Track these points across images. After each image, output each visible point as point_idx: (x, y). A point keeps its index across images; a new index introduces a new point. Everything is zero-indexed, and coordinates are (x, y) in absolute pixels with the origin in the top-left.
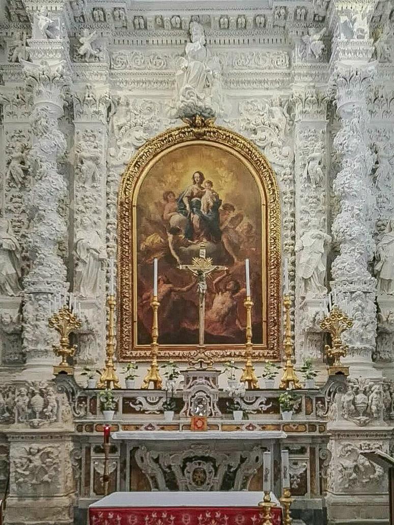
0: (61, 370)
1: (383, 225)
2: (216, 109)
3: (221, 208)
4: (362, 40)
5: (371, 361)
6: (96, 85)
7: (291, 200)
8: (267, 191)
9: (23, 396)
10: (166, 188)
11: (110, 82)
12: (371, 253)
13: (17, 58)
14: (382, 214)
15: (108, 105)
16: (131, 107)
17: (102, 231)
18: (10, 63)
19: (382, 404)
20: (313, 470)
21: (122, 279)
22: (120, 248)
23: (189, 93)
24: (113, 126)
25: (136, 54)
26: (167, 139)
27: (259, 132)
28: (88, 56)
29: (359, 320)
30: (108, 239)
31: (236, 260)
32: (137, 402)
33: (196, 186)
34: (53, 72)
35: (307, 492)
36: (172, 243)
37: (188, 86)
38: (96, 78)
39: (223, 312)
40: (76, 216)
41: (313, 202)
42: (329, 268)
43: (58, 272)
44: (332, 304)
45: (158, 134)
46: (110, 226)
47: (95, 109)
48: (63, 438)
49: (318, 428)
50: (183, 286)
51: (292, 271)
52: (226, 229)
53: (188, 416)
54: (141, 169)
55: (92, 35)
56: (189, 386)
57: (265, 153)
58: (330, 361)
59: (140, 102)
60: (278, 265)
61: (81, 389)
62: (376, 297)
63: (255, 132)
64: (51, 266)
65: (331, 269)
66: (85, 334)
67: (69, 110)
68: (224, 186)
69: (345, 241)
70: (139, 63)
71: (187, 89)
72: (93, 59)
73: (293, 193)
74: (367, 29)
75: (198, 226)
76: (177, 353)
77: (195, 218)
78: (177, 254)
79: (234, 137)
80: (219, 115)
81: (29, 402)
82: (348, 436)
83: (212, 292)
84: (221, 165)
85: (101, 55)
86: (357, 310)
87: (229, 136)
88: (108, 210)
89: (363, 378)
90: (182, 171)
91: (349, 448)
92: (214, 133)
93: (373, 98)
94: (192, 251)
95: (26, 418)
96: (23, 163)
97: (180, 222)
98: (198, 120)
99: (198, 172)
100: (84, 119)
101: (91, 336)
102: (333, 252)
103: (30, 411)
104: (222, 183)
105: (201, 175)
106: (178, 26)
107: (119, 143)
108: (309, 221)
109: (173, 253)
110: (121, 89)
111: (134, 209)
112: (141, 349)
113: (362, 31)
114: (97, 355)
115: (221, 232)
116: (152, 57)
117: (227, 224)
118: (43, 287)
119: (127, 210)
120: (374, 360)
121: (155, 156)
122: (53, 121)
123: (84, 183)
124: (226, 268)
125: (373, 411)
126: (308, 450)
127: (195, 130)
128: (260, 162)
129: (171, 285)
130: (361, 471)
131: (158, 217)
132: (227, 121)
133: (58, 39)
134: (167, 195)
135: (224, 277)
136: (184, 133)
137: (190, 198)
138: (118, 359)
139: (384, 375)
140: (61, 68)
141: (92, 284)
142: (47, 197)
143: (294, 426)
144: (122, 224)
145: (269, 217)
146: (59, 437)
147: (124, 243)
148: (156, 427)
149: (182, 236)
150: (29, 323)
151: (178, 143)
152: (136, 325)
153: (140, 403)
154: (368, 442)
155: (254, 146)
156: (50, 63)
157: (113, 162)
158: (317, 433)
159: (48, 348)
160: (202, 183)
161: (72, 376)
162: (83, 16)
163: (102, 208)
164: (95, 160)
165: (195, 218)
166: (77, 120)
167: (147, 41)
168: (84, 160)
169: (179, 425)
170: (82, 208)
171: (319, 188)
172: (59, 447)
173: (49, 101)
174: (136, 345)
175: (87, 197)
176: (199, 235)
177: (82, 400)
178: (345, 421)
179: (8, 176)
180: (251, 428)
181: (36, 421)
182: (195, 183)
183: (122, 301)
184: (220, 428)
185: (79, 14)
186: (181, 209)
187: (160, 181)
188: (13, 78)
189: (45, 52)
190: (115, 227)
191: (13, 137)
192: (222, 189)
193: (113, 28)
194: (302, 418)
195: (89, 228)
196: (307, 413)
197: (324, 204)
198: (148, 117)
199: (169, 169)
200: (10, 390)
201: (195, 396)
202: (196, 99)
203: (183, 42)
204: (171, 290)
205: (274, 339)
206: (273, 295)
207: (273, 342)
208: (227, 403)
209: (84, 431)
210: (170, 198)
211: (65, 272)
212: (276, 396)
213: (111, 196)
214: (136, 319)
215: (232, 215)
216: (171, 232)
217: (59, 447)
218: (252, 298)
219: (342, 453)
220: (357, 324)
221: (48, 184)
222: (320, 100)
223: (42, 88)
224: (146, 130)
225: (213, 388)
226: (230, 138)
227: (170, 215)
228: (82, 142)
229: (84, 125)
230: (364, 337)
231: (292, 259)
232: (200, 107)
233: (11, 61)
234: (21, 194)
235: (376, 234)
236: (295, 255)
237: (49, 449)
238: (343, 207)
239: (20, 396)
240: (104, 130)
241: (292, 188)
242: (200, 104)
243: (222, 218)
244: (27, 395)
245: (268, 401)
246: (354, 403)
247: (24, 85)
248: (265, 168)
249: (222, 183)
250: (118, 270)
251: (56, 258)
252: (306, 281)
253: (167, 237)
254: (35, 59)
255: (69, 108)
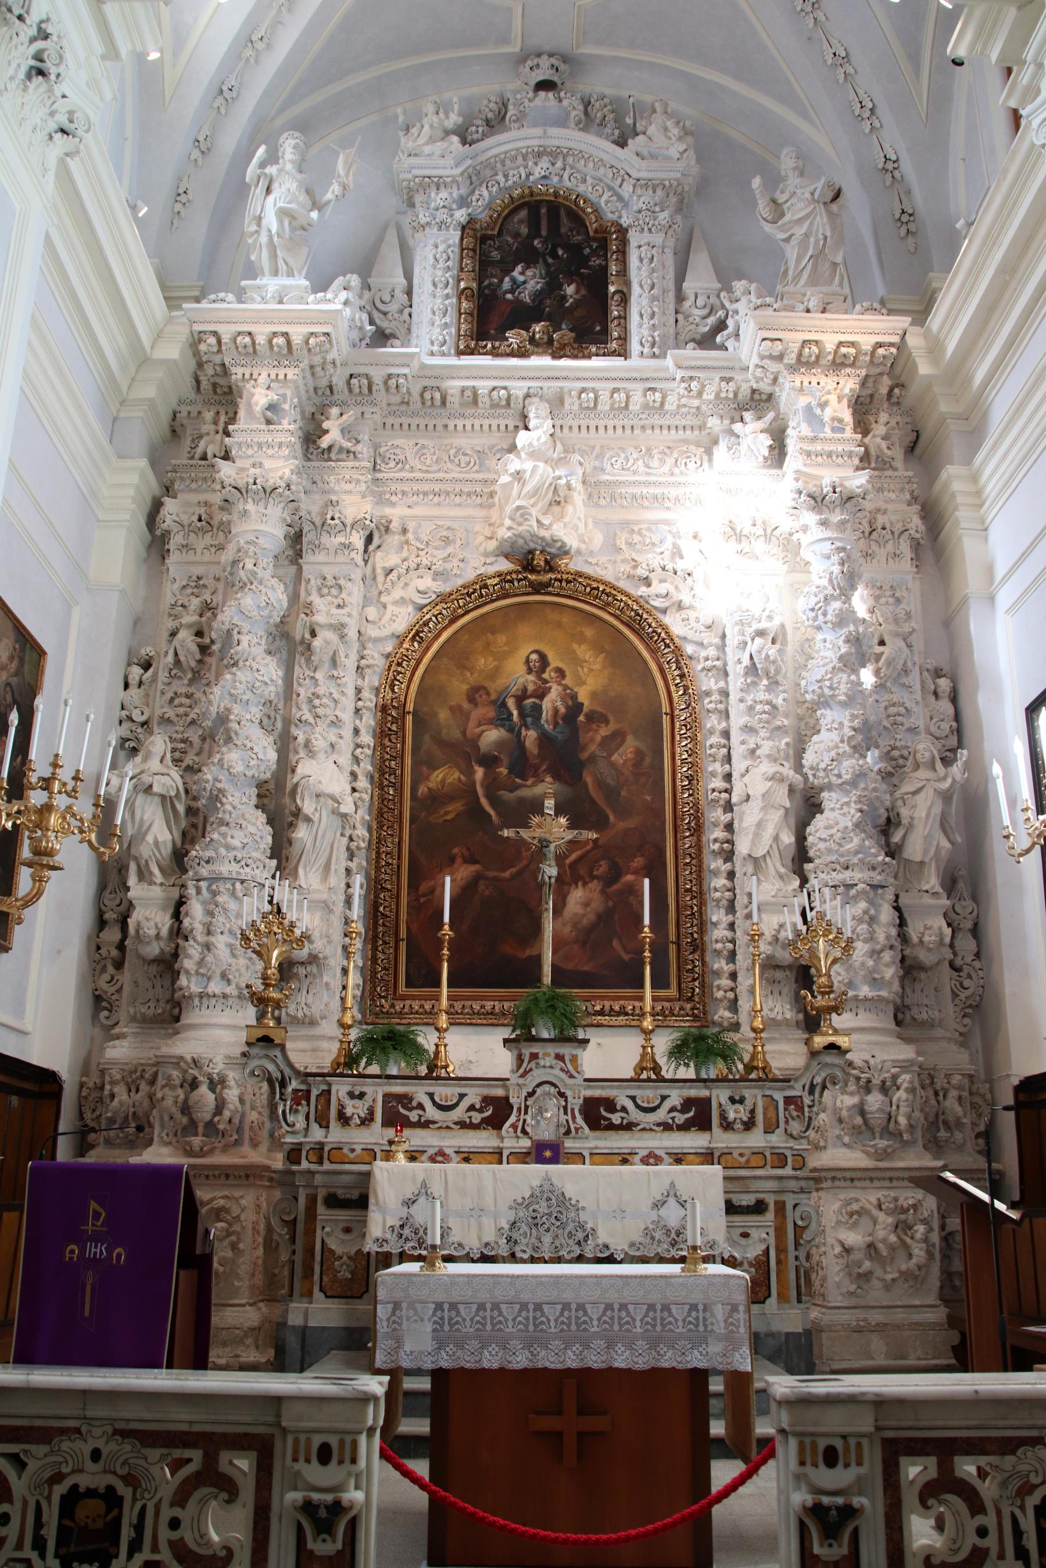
0: (260, 1033)
1: (902, 757)
2: (572, 542)
3: (581, 718)
4: (839, 436)
5: (892, 1025)
6: (347, 499)
7: (721, 707)
8: (673, 688)
9: (173, 1088)
10: (473, 679)
11: (373, 493)
12: (882, 811)
13: (205, 454)
14: (898, 737)
15: (367, 533)
16: (410, 536)
17: (345, 760)
18: (191, 462)
19: (917, 1114)
20: (781, 1250)
21: (378, 853)
22: (377, 792)
23: (522, 516)
24: (374, 570)
25: (424, 447)
26: (477, 591)
27: (654, 583)
28: (335, 450)
29: (865, 941)
30: (354, 775)
31: (612, 818)
32: (414, 1104)
33: (531, 678)
34: (274, 479)
35: (769, 1296)
36: (482, 784)
37: (518, 503)
38: (348, 487)
39: (585, 922)
40: (295, 731)
41: (765, 712)
42: (801, 838)
43: (258, 838)
44: (811, 909)
45: (460, 582)
46: (359, 750)
47: (343, 540)
48: (251, 1179)
49: (790, 1160)
50: (504, 870)
51: (727, 842)
52: (592, 759)
53: (519, 1134)
54: (424, 645)
55: (345, 417)
56: (521, 1071)
57: (667, 620)
58: (811, 1023)
59: (427, 527)
60: (698, 830)
61: (297, 1073)
62: (897, 896)
63: (647, 582)
64: (245, 831)
65: (805, 839)
66: (302, 963)
67: (296, 542)
68: (589, 679)
69: (829, 787)
70: (428, 462)
71: (519, 508)
72: (344, 456)
73: (725, 693)
74: (847, 416)
75: (536, 751)
76: (489, 1005)
77: (530, 736)
78: (493, 804)
79: (608, 590)
80: (579, 552)
81: (186, 1100)
82: (852, 1180)
83: (563, 885)
84: (582, 639)
85: (359, 448)
86: (860, 921)
87: (597, 589)
88: (358, 722)
89: (879, 1058)
90: (506, 648)
91: (855, 1207)
92: (568, 582)
93: (868, 530)
94: (522, 800)
95: (176, 1135)
96: (199, 634)
97: (500, 744)
98: (539, 561)
99: (536, 652)
100: (321, 557)
101: (314, 969)
102: (808, 805)
103: (185, 1120)
104: (583, 672)
105: (543, 659)
106: (504, 403)
107: (383, 599)
108: (758, 747)
109: (484, 802)
110: (393, 504)
111: (409, 719)
112: (413, 998)
113: (840, 421)
114: (322, 1007)
115: (582, 765)
116: (452, 452)
117: (593, 748)
118: (226, 868)
119: (395, 720)
120: (898, 1023)
121: (453, 621)
122: (267, 561)
123: (315, 671)
124: (595, 836)
125: (902, 1128)
126: (772, 1207)
127: (532, 577)
128: (659, 635)
129: (474, 868)
130: (881, 1255)
131: (456, 734)
132: (594, 561)
133: (285, 424)
134: (474, 694)
135: (588, 852)
136: (511, 581)
137: (520, 699)
138: (364, 1015)
139: (918, 1053)
140: (287, 472)
141: (322, 861)
142: (245, 698)
143: (741, 1155)
144: (383, 747)
145: (678, 737)
146: (248, 1175)
147: (386, 783)
148: (453, 1155)
149: (503, 771)
150: (195, 940)
151: (498, 599)
152: (403, 946)
153: (624, 1109)
154: (892, 1194)
155: (646, 606)
156: (268, 464)
157: (372, 632)
158: (788, 1171)
159: (228, 990)
160: (544, 672)
161: (282, 1047)
162: (331, 387)
163: (347, 716)
164: (339, 628)
165: (530, 736)
166: (308, 557)
167: (446, 426)
168: (317, 629)
169: (501, 1154)
170: (308, 716)
171: (774, 687)
172: (242, 1197)
173: (262, 528)
174: (402, 989)
175: (318, 697)
176: (536, 768)
177: (302, 1097)
178: (843, 1150)
179: (170, 658)
180: (652, 1161)
181: (197, 1141)
182: (530, 671)
183: (377, 897)
184: (587, 1161)
185: (324, 383)
186: (502, 718)
187: (462, 667)
188: (194, 486)
189: (260, 446)
190: (369, 752)
191: (184, 587)
192: (584, 683)
193: (384, 405)
194: (756, 1139)
195: (322, 756)
196: (768, 1130)
197: (786, 716)
198: (441, 554)
199: (479, 645)
200: (142, 1077)
201: (534, 1092)
202: (535, 524)
203: (511, 428)
204: (477, 879)
205: (694, 980)
206: (690, 890)
207: (691, 985)
208: (649, 798)
209: (326, 1162)
210: (481, 698)
211: (270, 840)
212: (704, 1093)
213: (366, 694)
214: (403, 934)
215: (604, 731)
216: (481, 763)
217: (242, 1197)
218: (650, 927)
219: (840, 1218)
220: (861, 948)
221: (249, 673)
222: (769, 532)
223: (250, 506)
224: (437, 575)
225: (571, 1076)
226: (602, 592)
227: (477, 730)
228: (315, 598)
229: (318, 567)
230: (876, 976)
231: (725, 818)
232: (543, 539)
233: (192, 458)
234: (192, 690)
235: (890, 774)
236: (732, 811)
237: (222, 1202)
238: (823, 722)
239: (167, 1089)
240: (357, 575)
241: (722, 684)
242: (546, 534)
243: (584, 737)
244: (182, 1086)
245: (688, 1104)
246: (862, 1113)
247: (216, 499)
248: (667, 646)
249: (583, 672)
250: (371, 835)
251: (253, 810)
252: (757, 863)
253: (474, 772)
254: (240, 457)
255: (296, 539)
